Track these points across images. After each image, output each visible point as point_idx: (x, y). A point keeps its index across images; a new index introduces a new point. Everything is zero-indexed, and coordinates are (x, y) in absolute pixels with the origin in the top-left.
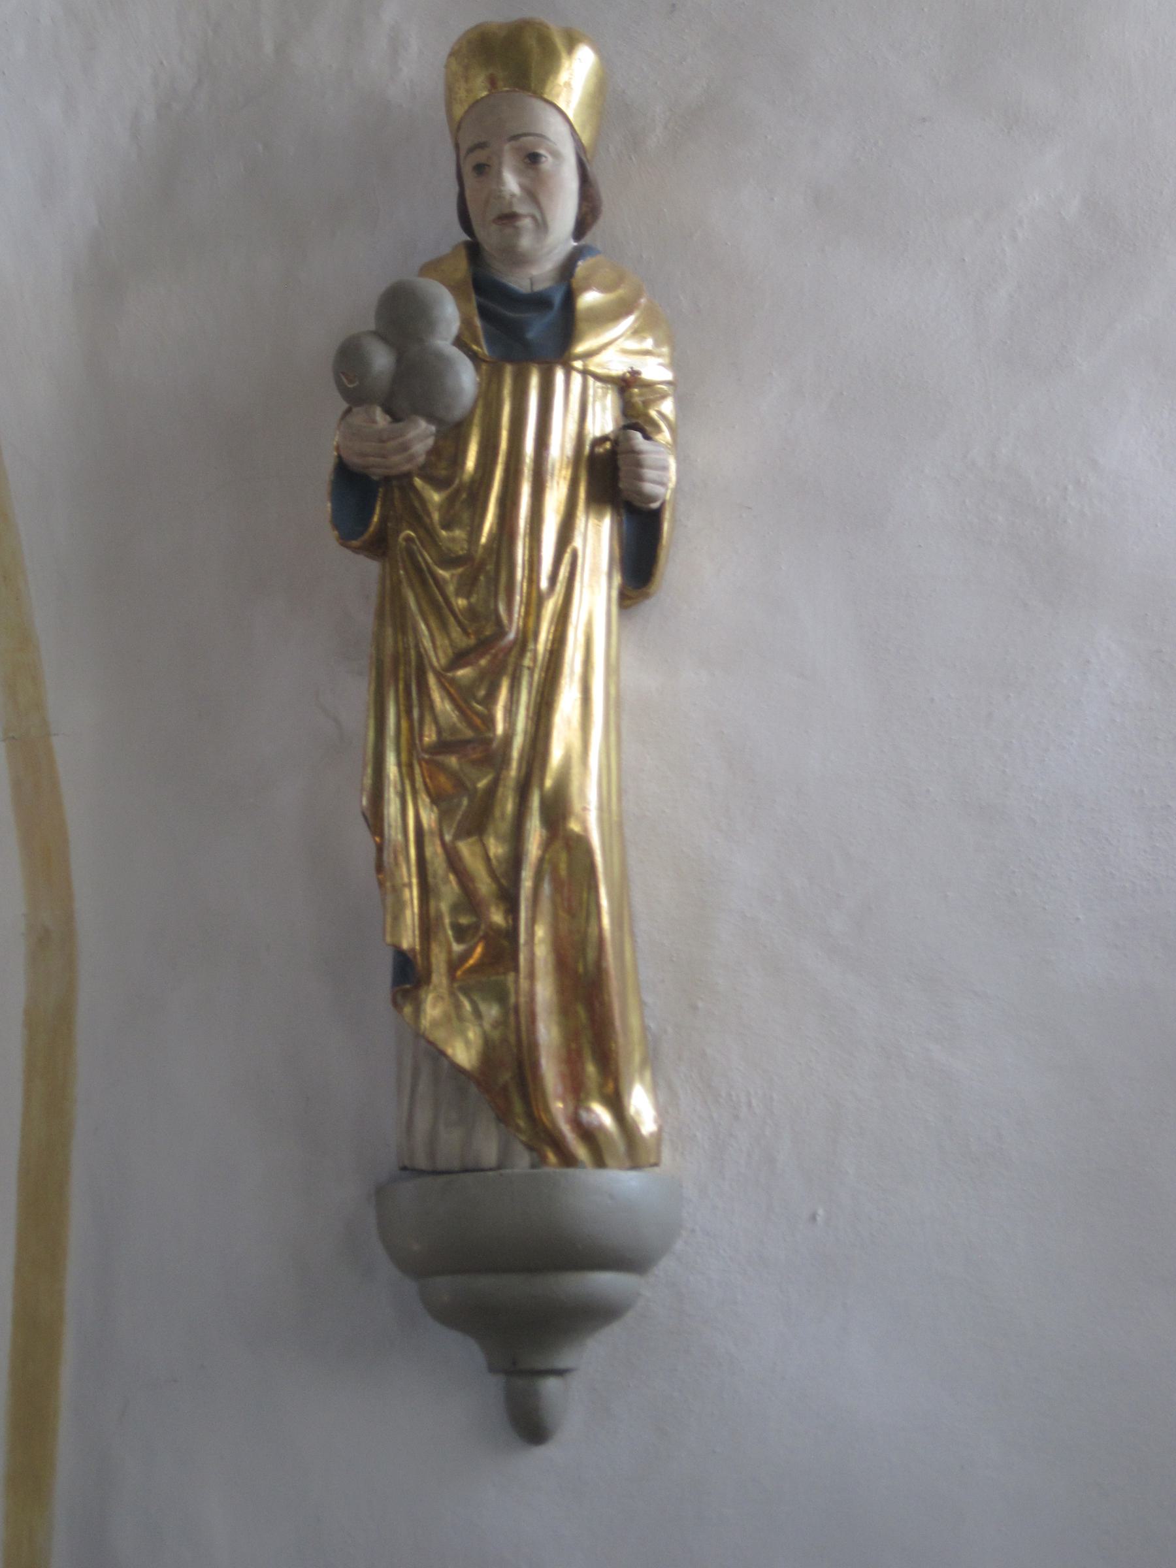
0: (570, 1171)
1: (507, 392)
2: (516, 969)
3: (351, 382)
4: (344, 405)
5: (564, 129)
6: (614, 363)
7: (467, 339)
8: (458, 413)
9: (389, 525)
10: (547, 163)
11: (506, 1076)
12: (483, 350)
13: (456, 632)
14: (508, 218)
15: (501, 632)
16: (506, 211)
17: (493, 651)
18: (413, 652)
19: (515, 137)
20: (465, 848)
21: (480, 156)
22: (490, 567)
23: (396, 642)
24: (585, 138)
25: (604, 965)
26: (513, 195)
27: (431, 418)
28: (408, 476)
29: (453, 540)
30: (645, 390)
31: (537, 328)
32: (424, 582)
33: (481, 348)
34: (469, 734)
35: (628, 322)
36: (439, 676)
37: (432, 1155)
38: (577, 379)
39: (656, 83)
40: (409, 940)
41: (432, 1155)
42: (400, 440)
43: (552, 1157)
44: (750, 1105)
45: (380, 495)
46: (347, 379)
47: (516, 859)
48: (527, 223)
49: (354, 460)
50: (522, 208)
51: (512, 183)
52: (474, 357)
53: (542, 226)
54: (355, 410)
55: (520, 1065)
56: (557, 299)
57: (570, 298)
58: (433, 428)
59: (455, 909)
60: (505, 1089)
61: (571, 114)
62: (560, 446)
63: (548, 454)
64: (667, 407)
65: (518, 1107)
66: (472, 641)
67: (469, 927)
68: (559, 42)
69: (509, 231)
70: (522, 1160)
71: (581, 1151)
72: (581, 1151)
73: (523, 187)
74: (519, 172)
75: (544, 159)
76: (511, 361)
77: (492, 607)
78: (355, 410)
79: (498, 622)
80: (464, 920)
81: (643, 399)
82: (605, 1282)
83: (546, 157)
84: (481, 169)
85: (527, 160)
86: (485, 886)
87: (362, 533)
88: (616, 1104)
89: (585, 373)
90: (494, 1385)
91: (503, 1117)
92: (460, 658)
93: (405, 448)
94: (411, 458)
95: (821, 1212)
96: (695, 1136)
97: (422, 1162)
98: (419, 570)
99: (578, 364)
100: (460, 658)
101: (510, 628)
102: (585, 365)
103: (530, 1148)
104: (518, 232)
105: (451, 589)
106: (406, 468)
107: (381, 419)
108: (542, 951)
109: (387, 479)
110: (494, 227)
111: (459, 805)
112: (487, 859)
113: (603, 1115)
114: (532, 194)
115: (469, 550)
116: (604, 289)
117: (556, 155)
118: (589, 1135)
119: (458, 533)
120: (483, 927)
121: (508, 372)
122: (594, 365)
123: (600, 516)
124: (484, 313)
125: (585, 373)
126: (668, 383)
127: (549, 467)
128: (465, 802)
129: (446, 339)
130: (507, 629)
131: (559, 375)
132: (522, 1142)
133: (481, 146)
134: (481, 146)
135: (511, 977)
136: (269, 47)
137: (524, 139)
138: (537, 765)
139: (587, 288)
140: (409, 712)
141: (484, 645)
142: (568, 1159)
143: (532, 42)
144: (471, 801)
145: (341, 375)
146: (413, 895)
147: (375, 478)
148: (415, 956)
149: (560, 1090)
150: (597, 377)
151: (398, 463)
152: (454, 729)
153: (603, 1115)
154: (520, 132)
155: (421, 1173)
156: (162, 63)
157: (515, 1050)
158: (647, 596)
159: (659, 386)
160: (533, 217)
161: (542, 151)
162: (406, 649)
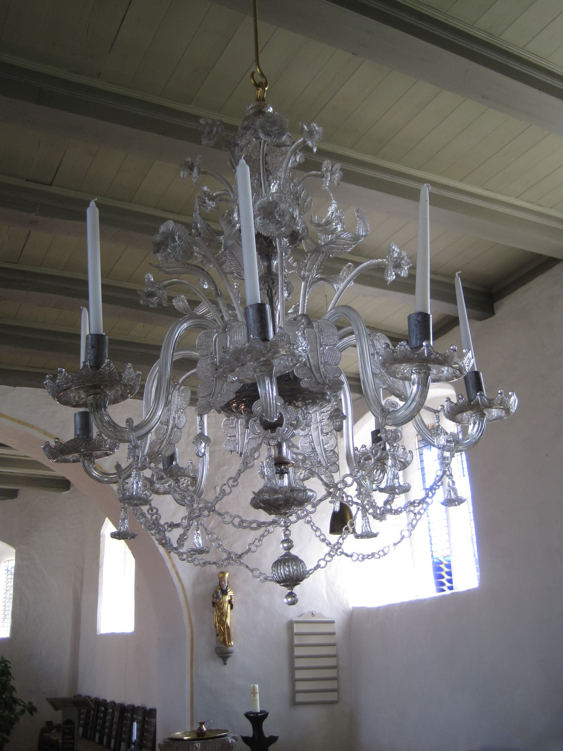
1: (149, 419)
4: (293, 552)
6: (230, 595)
14: (223, 585)
31: (225, 593)
33: (424, 349)
51: (223, 583)
62: (227, 600)
68: (312, 141)
70: (225, 647)
75: (278, 375)
82: (230, 654)
84: (221, 582)
88: (231, 643)
90: (223, 661)
91: (224, 644)
107: (215, 599)
113: (230, 644)
118: (229, 645)
142: (228, 647)
153: (230, 644)
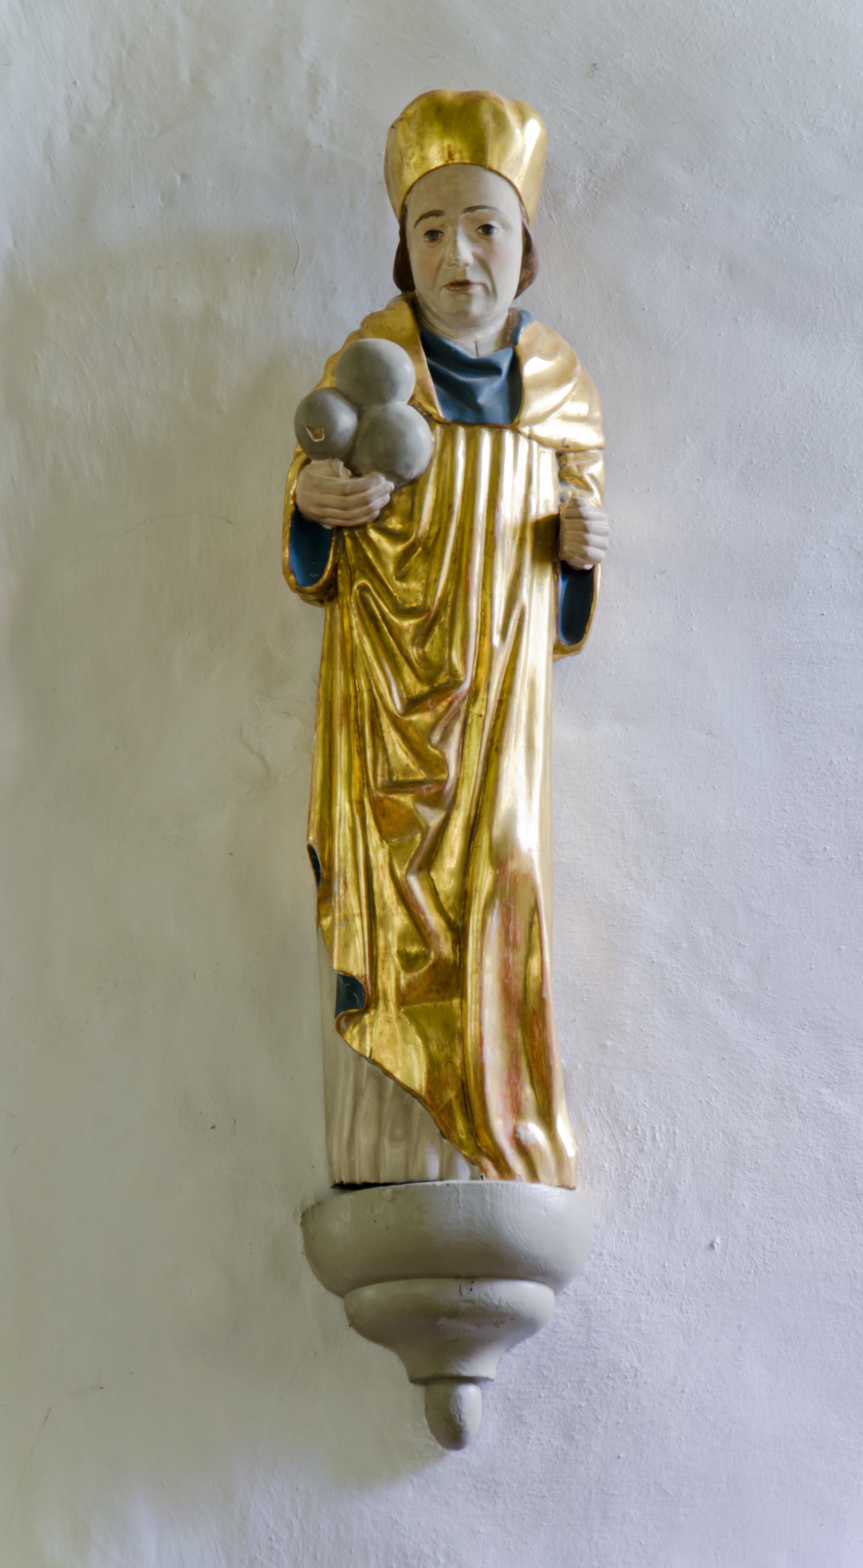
0: (510, 1183)
2: (463, 996)
3: (316, 436)
5: (515, 201)
7: (420, 399)
8: (415, 472)
9: (339, 572)
10: (498, 234)
11: (451, 1094)
12: (439, 412)
13: (409, 678)
14: (463, 285)
15: (455, 682)
16: (460, 278)
17: (450, 699)
18: (365, 695)
19: (471, 209)
20: (415, 884)
21: (433, 223)
22: (445, 619)
23: (347, 685)
24: (530, 207)
25: (545, 995)
26: (466, 265)
27: (391, 474)
28: (363, 527)
29: (408, 591)
30: (579, 454)
32: (378, 629)
34: (421, 776)
35: (568, 388)
36: (395, 722)
37: (376, 1168)
38: (523, 443)
39: (577, 143)
40: (357, 967)
41: (376, 1168)
42: (361, 495)
43: (492, 1171)
44: (654, 1137)
45: (333, 544)
46: (313, 433)
47: (464, 897)
48: (477, 290)
49: (311, 510)
50: (474, 276)
51: (466, 251)
52: (429, 417)
53: (491, 292)
54: (314, 462)
55: (464, 1085)
56: (505, 366)
57: (516, 365)
58: (391, 485)
59: (403, 938)
60: (449, 1106)
61: (519, 186)
63: (501, 515)
64: (596, 469)
65: (461, 1124)
66: (426, 689)
67: (417, 957)
68: (512, 117)
69: (462, 297)
70: (464, 1175)
71: (517, 1164)
72: (517, 1164)
73: (476, 256)
74: (472, 240)
76: (465, 424)
77: (446, 656)
78: (314, 462)
79: (453, 673)
80: (414, 949)
81: (577, 463)
83: (497, 229)
85: (480, 231)
86: (434, 921)
87: (316, 580)
89: (530, 437)
91: (446, 1133)
92: (413, 704)
93: (366, 502)
94: (371, 511)
95: (718, 1240)
96: (603, 1166)
97: (363, 1174)
98: (373, 618)
99: (526, 430)
100: (413, 704)
101: (465, 678)
102: (531, 430)
103: (472, 1162)
104: (470, 296)
105: (408, 637)
106: (362, 520)
108: (491, 981)
109: (339, 529)
110: (445, 291)
111: (412, 840)
112: (434, 893)
114: (484, 264)
115: (425, 602)
116: (549, 355)
117: (506, 226)
119: (415, 585)
120: (432, 955)
121: (461, 432)
122: (539, 430)
123: (542, 572)
124: (436, 375)
125: (530, 437)
126: (600, 448)
127: (501, 527)
128: (418, 837)
129: (404, 400)
130: (462, 678)
131: (508, 436)
132: (465, 1156)
133: (436, 213)
134: (436, 213)
135: (456, 1002)
136: (185, 75)
137: (478, 211)
138: (487, 806)
139: (530, 356)
140: (362, 752)
141: (438, 692)
142: (504, 1170)
143: (487, 117)
144: (423, 838)
145: (307, 429)
146: (359, 924)
147: (328, 527)
148: (366, 982)
149: (501, 1109)
150: (542, 443)
151: (357, 515)
152: (406, 771)
153: (534, 1132)
154: (475, 204)
155: (366, 1185)
156: (75, 83)
157: (459, 1072)
158: (578, 650)
159: (592, 451)
160: (484, 285)
161: (493, 223)
162: (358, 693)
